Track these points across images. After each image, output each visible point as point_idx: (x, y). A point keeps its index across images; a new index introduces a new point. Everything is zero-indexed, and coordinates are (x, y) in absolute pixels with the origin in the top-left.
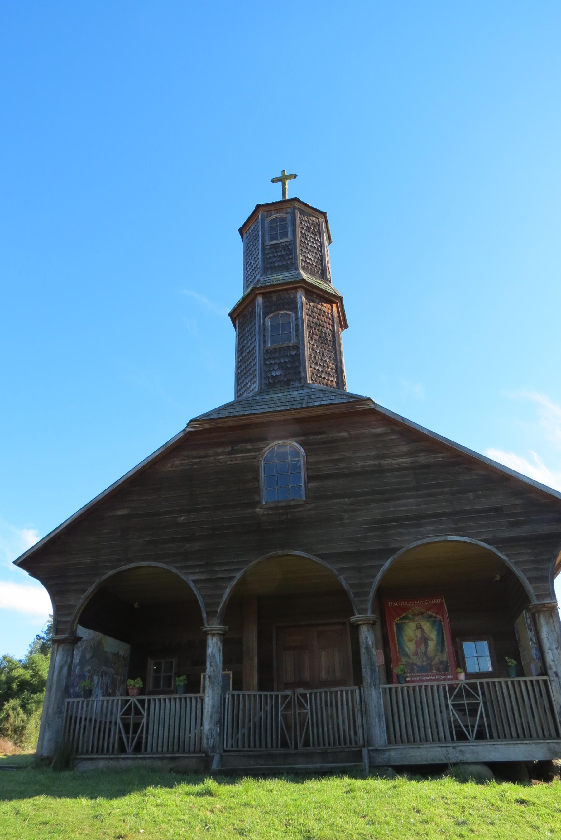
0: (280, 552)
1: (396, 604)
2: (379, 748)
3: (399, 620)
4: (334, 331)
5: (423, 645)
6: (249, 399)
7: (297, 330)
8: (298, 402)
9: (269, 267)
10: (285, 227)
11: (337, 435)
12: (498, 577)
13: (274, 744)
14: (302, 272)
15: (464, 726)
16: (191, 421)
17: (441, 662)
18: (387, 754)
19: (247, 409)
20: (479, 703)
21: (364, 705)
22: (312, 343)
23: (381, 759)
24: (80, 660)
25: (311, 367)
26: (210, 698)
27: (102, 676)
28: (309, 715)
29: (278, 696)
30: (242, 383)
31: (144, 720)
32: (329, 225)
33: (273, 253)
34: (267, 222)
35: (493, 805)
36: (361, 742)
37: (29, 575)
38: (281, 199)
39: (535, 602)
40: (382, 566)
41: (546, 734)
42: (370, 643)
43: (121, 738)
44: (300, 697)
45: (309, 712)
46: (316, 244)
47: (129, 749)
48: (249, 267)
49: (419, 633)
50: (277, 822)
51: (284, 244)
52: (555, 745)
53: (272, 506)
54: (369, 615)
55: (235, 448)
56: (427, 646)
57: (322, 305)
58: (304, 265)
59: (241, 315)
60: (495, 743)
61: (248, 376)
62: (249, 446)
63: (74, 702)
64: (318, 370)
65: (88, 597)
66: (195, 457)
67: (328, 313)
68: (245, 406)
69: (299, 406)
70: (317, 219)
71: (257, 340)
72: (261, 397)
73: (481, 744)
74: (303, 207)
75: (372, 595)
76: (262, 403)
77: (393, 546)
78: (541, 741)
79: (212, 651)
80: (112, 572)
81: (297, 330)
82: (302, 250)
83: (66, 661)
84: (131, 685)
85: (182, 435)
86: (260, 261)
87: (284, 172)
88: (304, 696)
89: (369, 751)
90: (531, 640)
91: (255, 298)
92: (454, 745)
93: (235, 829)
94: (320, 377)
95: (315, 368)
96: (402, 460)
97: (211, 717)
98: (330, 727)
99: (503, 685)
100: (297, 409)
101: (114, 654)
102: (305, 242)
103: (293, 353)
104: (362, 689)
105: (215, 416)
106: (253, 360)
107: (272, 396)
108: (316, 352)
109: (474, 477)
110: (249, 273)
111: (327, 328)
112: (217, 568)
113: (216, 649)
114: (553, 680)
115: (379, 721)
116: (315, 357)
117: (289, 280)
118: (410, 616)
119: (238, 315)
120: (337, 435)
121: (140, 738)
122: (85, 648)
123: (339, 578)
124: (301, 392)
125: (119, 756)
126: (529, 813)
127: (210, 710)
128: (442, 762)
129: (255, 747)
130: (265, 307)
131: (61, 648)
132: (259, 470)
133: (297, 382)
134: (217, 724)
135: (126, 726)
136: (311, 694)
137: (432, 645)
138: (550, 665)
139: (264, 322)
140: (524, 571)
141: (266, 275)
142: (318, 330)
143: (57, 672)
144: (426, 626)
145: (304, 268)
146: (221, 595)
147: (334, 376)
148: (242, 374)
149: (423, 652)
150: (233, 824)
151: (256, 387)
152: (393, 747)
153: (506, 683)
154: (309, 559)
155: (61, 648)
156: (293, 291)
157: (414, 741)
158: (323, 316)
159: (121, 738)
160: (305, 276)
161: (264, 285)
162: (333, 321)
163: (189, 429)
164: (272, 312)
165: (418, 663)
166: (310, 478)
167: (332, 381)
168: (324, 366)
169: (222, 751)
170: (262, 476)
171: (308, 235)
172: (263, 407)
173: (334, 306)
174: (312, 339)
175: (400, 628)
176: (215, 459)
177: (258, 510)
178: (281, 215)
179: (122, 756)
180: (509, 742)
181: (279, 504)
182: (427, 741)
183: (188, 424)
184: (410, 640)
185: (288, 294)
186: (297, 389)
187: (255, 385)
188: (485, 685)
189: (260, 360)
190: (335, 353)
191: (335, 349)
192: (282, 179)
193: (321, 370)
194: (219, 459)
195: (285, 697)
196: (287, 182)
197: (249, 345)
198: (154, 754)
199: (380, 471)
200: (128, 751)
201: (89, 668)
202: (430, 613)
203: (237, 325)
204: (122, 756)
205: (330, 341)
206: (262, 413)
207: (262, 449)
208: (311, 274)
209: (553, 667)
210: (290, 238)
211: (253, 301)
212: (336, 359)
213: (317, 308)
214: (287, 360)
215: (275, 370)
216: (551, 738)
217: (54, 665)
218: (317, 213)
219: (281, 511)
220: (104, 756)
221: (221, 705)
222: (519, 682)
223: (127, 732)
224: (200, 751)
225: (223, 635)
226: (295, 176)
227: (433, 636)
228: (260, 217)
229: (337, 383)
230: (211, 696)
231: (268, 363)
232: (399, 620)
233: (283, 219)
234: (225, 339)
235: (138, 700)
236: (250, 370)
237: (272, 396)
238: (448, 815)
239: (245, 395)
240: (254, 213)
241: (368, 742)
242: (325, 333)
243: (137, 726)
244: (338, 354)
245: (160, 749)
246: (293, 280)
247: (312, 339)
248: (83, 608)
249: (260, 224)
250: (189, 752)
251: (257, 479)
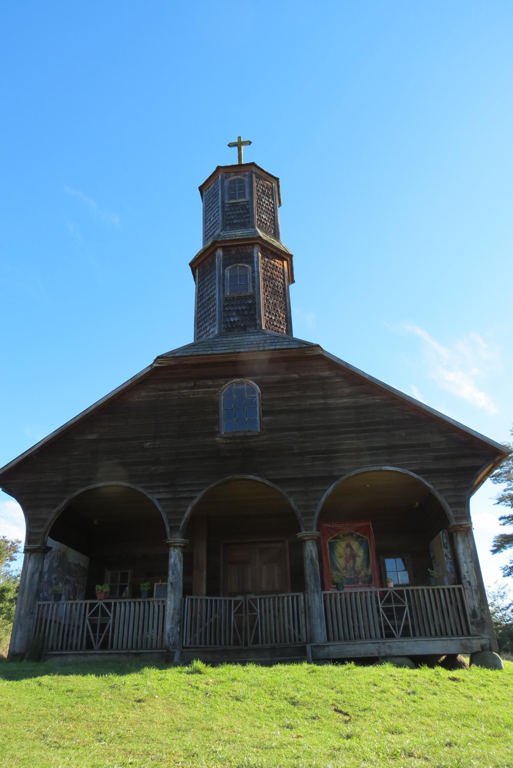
0: (237, 476)
1: (329, 526)
2: (320, 645)
3: (332, 539)
4: (285, 284)
5: (352, 561)
6: (210, 341)
7: (254, 282)
8: (255, 346)
9: (228, 224)
10: (242, 188)
11: (289, 376)
12: (417, 504)
13: (227, 642)
14: (258, 230)
15: (392, 626)
16: (158, 358)
17: (367, 576)
18: (327, 649)
19: (208, 349)
20: (405, 607)
21: (307, 609)
22: (266, 294)
23: (321, 654)
24: (48, 568)
25: (265, 315)
26: (171, 603)
27: (65, 584)
28: (259, 617)
29: (231, 600)
30: (201, 326)
31: (111, 621)
32: (281, 189)
33: (232, 211)
34: (226, 183)
35: (432, 681)
36: (305, 640)
37: (2, 490)
38: (237, 163)
39: (454, 523)
40: (326, 490)
41: (459, 632)
42: (314, 556)
43: (88, 637)
44: (250, 601)
45: (259, 615)
46: (270, 205)
47: (96, 646)
48: (209, 222)
49: (348, 551)
50: (263, 692)
52: (466, 641)
54: (314, 532)
55: (198, 384)
56: (355, 562)
57: (275, 261)
58: (260, 224)
59: (200, 266)
60: (418, 639)
61: (207, 320)
62: (210, 383)
63: (44, 605)
64: (271, 318)
65: (59, 511)
66: (161, 390)
67: (280, 269)
68: (207, 346)
69: (256, 349)
70: (270, 184)
71: (217, 289)
72: (221, 339)
73: (406, 640)
74: (259, 172)
75: (317, 515)
76: (223, 345)
77: (335, 474)
78: (456, 638)
79: (174, 561)
81: (254, 282)
82: (258, 210)
83: (37, 569)
84: (99, 590)
85: (149, 369)
86: (220, 217)
87: (239, 138)
88: (254, 601)
89: (312, 646)
90: (446, 556)
91: (215, 250)
92: (384, 641)
93: (231, 696)
94: (273, 324)
95: (268, 317)
96: (345, 400)
97: (173, 618)
98: (277, 627)
99: (425, 591)
100: (255, 351)
101: (76, 565)
102: (260, 203)
103: (250, 302)
104: (306, 594)
105: (179, 354)
106: (213, 306)
107: (231, 339)
108: (269, 302)
109: (407, 417)
110: (209, 227)
111: (279, 282)
112: (179, 489)
113: (177, 560)
114: (467, 588)
115: (321, 622)
116: (268, 306)
117: (247, 237)
118: (341, 536)
119: (198, 265)
120: (289, 376)
121: (107, 636)
122: (53, 558)
123: (289, 500)
124: (257, 337)
125: (88, 652)
126: (461, 687)
127: (171, 612)
128: (373, 656)
129: (210, 644)
130: (224, 260)
131: (32, 557)
132: (219, 404)
133: (253, 328)
134: (178, 624)
135: (94, 627)
136: (260, 599)
137: (359, 561)
138: (465, 576)
140: (445, 498)
141: (225, 231)
142: (272, 283)
143: (29, 577)
144: (355, 545)
145: (259, 226)
146: (184, 513)
147: (284, 324)
148: (202, 318)
149: (352, 567)
150: (229, 693)
151: (215, 330)
152: (333, 644)
153: (428, 590)
154: (263, 483)
155: (32, 557)
156: (250, 247)
157: (350, 639)
158: (276, 271)
159: (88, 637)
160: (261, 234)
161: (224, 239)
162: (284, 276)
163: (156, 365)
164: (231, 264)
165: (347, 577)
166: (264, 413)
167: (282, 329)
168: (276, 315)
169: (182, 648)
170: (222, 408)
171: (263, 197)
172: (224, 348)
173: (285, 263)
174: (266, 290)
175: (332, 546)
176: (179, 392)
177: (217, 439)
178: (239, 177)
179: (90, 652)
180: (428, 639)
181: (237, 435)
182: (360, 638)
183: (155, 360)
184: (341, 557)
185: (246, 249)
186: (253, 334)
187: (214, 329)
188: (410, 592)
189: (220, 306)
190: (286, 305)
191: (285, 301)
192: (238, 145)
193: (273, 318)
194: (182, 393)
195: (236, 603)
196: (243, 148)
197: (209, 292)
198: (120, 650)
200: (95, 648)
201: (55, 575)
202: (358, 534)
203: (197, 274)
204: (90, 652)
205: (281, 293)
206: (224, 354)
207: (221, 385)
208: (265, 232)
209: (467, 577)
210: (247, 198)
211: (213, 253)
212: (286, 310)
213: (271, 264)
214: (244, 308)
215: (234, 317)
216: (463, 635)
217: (27, 571)
218: (270, 178)
219: (238, 441)
220: (77, 652)
221: (181, 608)
222: (438, 590)
223: (94, 631)
224: (161, 648)
225: (184, 547)
226: (250, 143)
227: (361, 553)
228: (220, 177)
229: (287, 331)
230: (172, 600)
231: (227, 309)
232: (332, 539)
233: (241, 181)
234: (187, 287)
235: (105, 603)
236: (209, 315)
237: (231, 339)
238: (398, 688)
239: (204, 337)
240: (214, 173)
241: (311, 639)
242: (278, 286)
243: (103, 626)
244: (288, 305)
245: (125, 646)
246: (251, 236)
247: (266, 290)
248: (54, 521)
249: (220, 184)
250: (152, 648)
251: (217, 412)
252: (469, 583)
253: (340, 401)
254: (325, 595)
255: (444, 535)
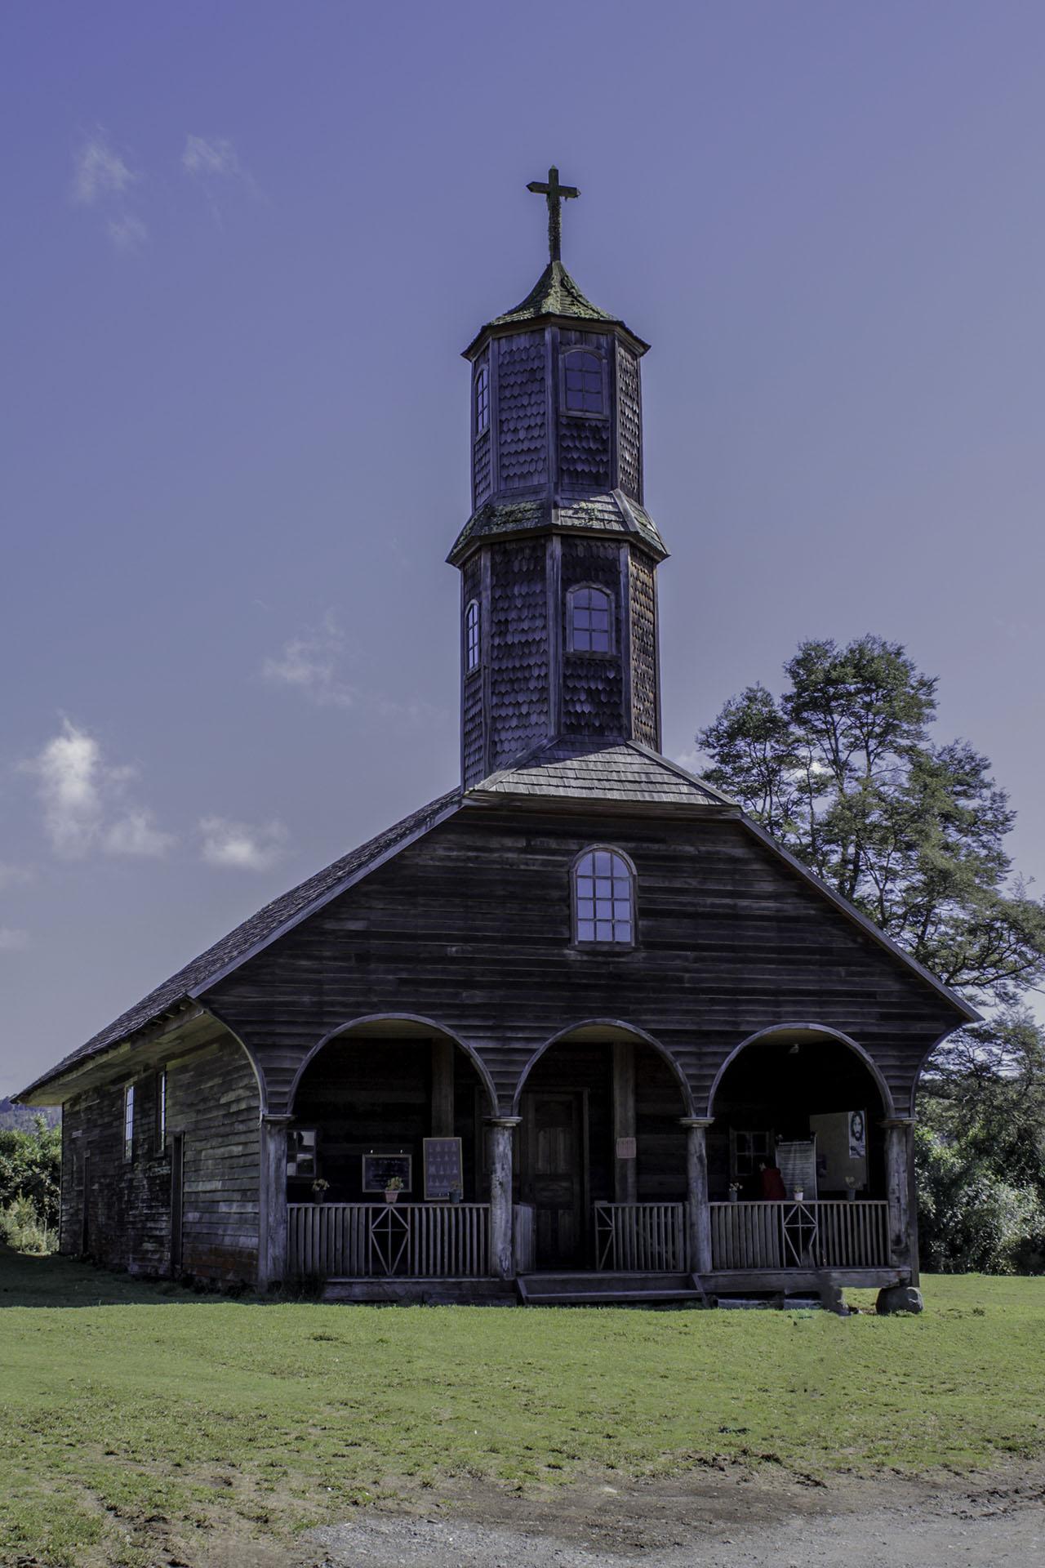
33: (572, 437)
51: (593, 423)
53: (588, 948)
77: (743, 1028)
80: (350, 1023)
130: (565, 564)
139: (564, 597)
140: (887, 1078)
199: (735, 917)
215: (582, 702)
252: (898, 1199)
253: (756, 905)
254: (712, 1208)
255: (858, 1120)
